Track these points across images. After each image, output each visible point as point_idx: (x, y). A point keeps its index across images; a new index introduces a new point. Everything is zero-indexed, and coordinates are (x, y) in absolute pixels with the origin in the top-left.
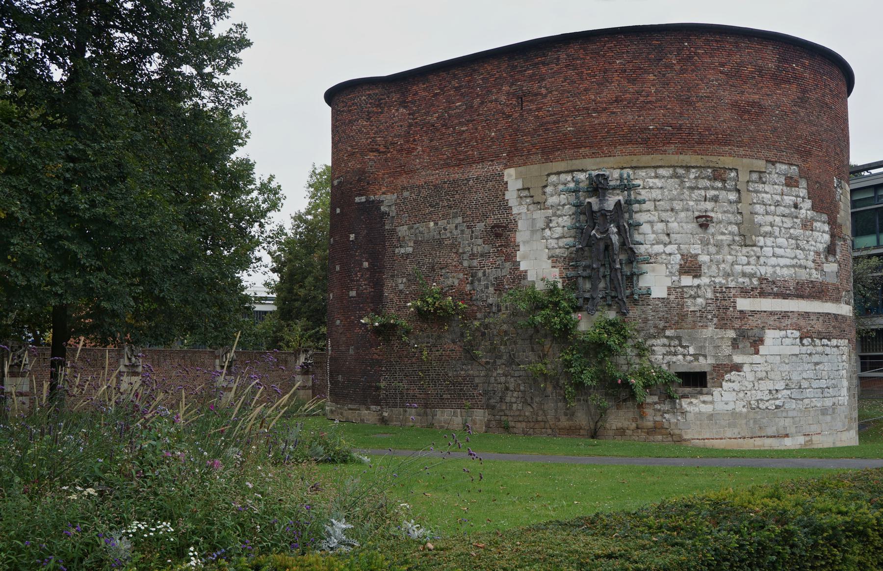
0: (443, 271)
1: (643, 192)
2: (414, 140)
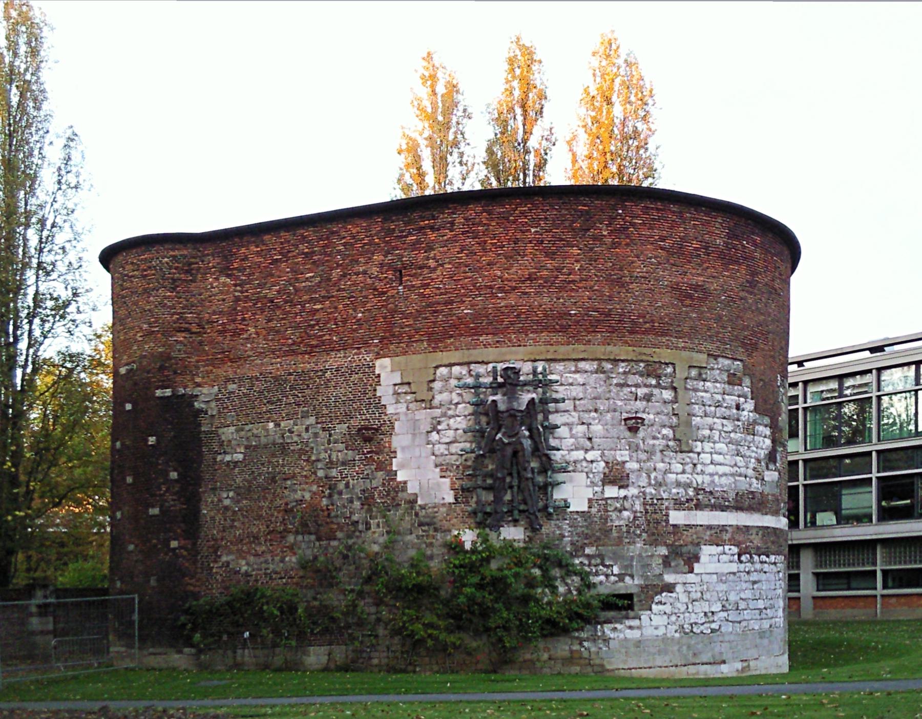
0: (289, 482)
1: (561, 389)
2: (244, 319)
